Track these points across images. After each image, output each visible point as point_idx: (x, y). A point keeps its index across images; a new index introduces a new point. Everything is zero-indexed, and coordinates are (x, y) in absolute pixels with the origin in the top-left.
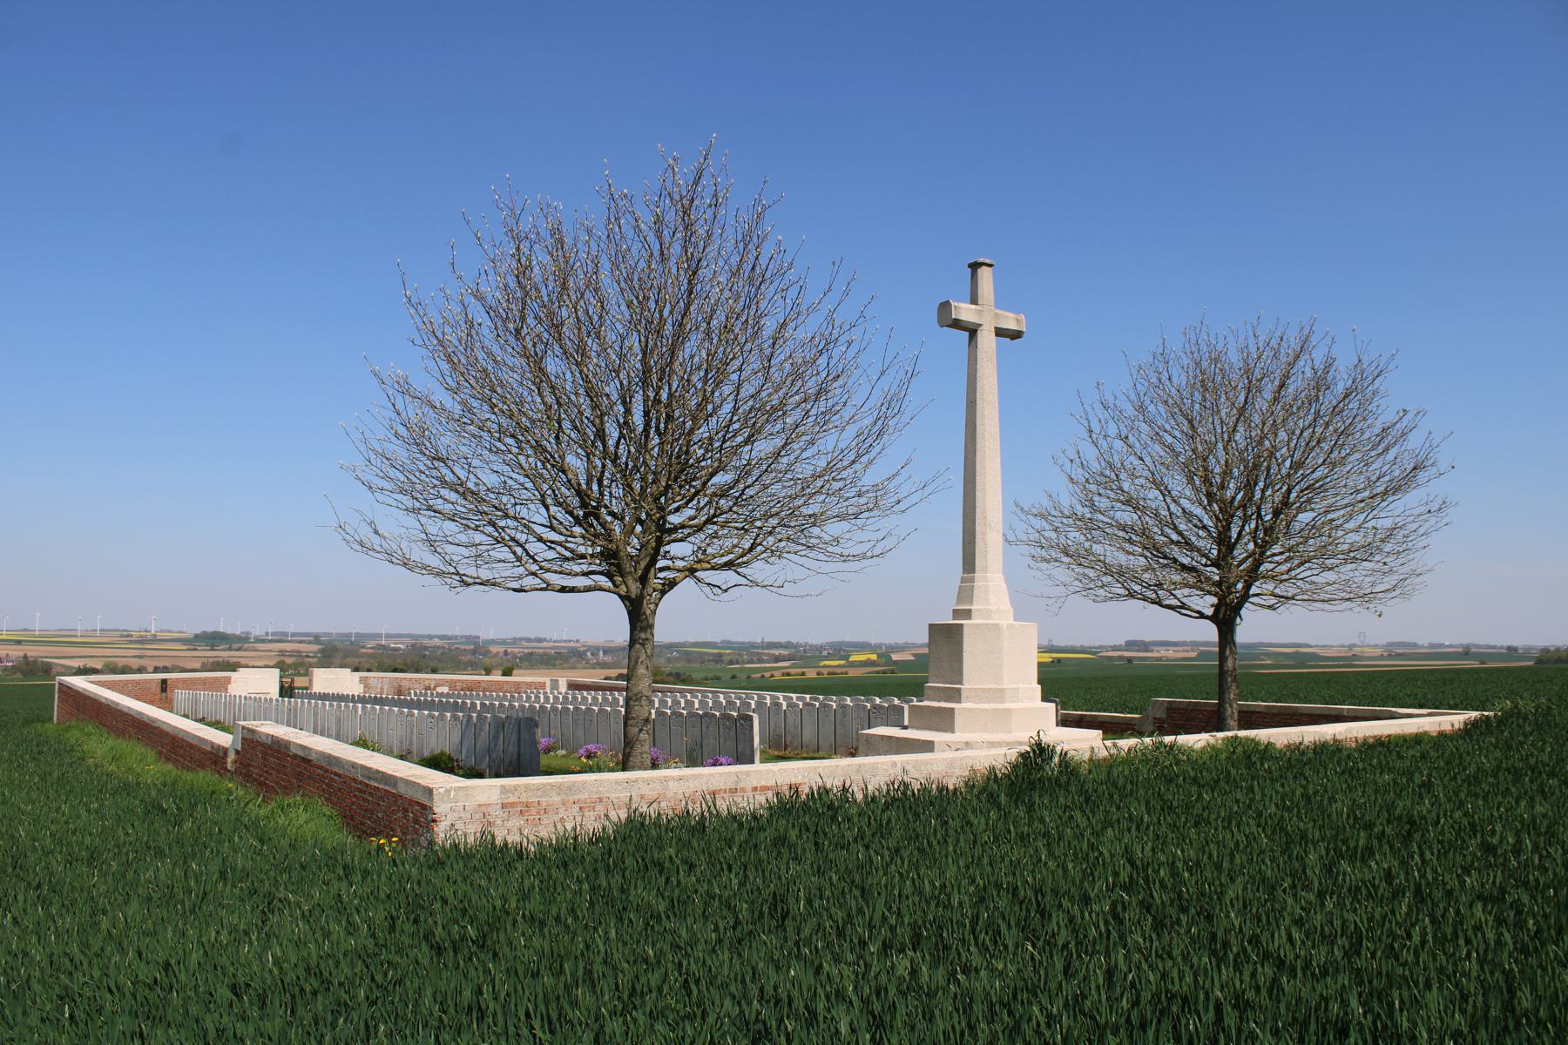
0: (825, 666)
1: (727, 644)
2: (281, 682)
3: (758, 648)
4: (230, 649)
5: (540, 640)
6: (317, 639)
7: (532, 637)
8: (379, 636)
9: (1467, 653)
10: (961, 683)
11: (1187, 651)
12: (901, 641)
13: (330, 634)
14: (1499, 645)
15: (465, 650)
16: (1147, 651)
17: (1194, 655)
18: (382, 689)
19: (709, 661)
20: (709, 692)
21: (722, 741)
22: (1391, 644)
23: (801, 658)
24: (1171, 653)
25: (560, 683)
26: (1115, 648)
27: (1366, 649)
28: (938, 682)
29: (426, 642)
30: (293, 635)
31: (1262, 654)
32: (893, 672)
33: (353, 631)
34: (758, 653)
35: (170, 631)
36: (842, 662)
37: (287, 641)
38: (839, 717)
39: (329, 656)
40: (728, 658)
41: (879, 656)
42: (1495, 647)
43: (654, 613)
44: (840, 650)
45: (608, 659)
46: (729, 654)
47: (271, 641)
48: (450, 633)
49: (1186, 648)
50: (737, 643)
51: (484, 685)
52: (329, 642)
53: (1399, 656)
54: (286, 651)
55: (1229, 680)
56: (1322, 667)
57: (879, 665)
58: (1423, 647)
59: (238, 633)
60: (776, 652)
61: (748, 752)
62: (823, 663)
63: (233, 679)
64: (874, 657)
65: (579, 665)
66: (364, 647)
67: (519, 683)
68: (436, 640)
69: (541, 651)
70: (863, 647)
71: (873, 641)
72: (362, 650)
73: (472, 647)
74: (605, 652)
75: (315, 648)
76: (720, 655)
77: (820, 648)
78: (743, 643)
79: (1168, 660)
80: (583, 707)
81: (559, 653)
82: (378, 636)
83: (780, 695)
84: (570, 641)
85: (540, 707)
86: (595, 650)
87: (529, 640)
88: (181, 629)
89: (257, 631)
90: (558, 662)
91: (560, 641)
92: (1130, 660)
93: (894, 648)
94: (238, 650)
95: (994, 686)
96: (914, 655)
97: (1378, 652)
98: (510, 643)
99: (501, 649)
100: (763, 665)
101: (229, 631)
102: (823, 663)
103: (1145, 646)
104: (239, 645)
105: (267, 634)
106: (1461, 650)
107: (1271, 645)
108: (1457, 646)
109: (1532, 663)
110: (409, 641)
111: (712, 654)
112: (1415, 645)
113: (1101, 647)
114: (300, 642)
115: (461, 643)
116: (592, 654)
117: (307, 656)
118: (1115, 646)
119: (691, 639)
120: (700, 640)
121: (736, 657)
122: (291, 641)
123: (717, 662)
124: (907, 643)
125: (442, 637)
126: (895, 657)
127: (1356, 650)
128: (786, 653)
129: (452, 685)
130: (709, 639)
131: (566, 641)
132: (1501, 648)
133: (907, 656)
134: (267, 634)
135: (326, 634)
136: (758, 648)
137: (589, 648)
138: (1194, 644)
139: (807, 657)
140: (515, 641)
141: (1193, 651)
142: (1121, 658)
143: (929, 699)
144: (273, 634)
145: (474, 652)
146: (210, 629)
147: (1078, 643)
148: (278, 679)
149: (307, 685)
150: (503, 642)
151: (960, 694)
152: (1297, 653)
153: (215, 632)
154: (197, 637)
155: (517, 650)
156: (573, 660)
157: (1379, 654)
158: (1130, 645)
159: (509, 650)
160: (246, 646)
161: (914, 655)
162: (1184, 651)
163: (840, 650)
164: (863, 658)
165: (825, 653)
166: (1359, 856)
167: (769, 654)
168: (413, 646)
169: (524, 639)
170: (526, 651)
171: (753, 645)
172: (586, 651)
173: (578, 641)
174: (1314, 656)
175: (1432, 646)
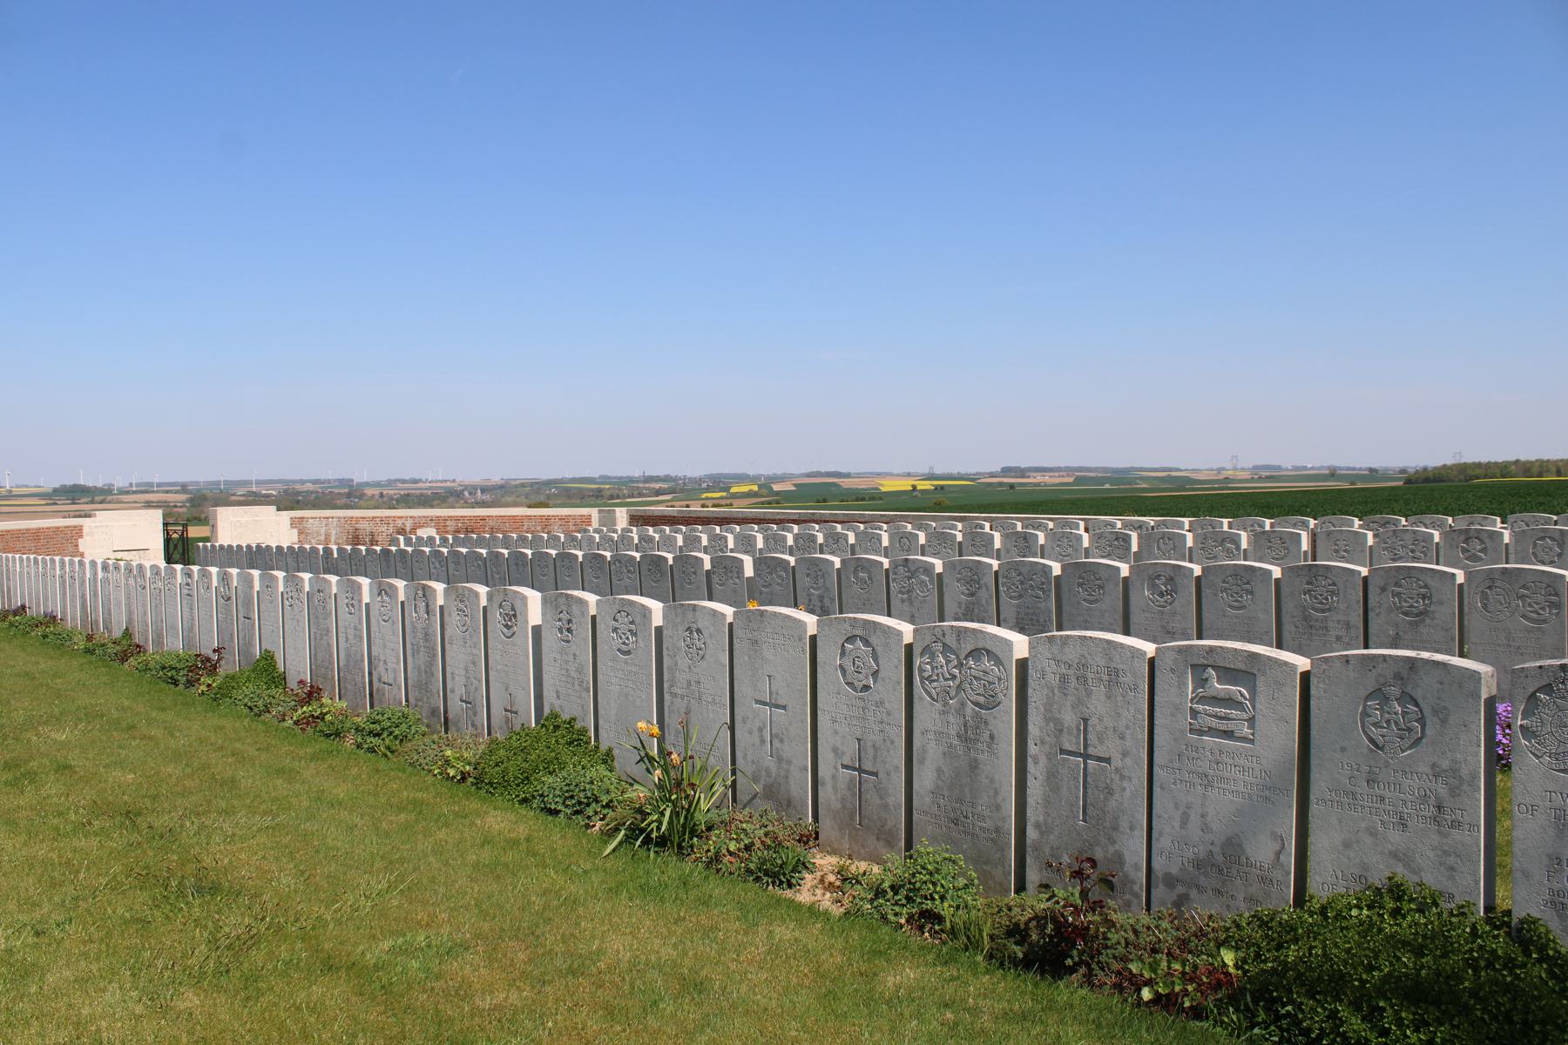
0: (707, 498)
1: (605, 479)
2: (166, 532)
3: (637, 482)
4: (92, 502)
5: (415, 481)
6: (184, 488)
7: (407, 478)
8: (249, 483)
9: (1333, 474)
11: (1063, 476)
12: (779, 472)
13: (197, 483)
14: (1358, 466)
15: (339, 493)
16: (1023, 477)
17: (1071, 480)
18: (327, 537)
19: (589, 496)
20: (1017, 519)
22: (1257, 468)
23: (682, 491)
25: (618, 514)
26: (992, 475)
29: (298, 487)
30: (159, 485)
31: (1137, 478)
33: (222, 479)
34: (638, 487)
35: (27, 486)
36: (724, 494)
37: (153, 492)
39: (199, 505)
40: (608, 493)
41: (760, 486)
42: (1354, 469)
44: (719, 482)
45: (487, 497)
46: (608, 489)
47: (134, 492)
48: (322, 477)
49: (1061, 474)
50: (615, 478)
51: (491, 523)
52: (198, 490)
54: (153, 502)
56: (1215, 489)
57: (762, 496)
58: (1287, 470)
59: (100, 485)
60: (657, 486)
62: (704, 495)
63: (85, 530)
64: (755, 488)
65: (457, 505)
66: (233, 495)
67: (548, 518)
68: (310, 485)
69: (418, 492)
70: (742, 478)
71: (751, 473)
72: (233, 498)
73: (347, 490)
74: (483, 491)
75: (183, 497)
76: (600, 490)
77: (700, 481)
78: (621, 478)
79: (1046, 485)
80: (553, 552)
81: (436, 493)
82: (248, 483)
84: (446, 481)
85: (367, 550)
86: (472, 489)
87: (404, 481)
88: (38, 484)
89: (120, 482)
90: (435, 503)
91: (436, 482)
92: (1012, 486)
93: (775, 478)
94: (101, 503)
98: (383, 486)
99: (376, 491)
100: (645, 499)
101: (90, 484)
102: (704, 495)
103: (1021, 472)
104: (102, 498)
105: (131, 485)
106: (1327, 472)
109: (1401, 483)
110: (281, 486)
111: (592, 490)
112: (1279, 468)
113: (978, 474)
114: (167, 492)
115: (336, 487)
116: (470, 494)
117: (175, 506)
118: (992, 473)
119: (568, 475)
120: (578, 476)
121: (617, 491)
122: (157, 492)
123: (597, 497)
124: (785, 474)
125: (315, 482)
126: (776, 488)
127: (1230, 473)
128: (666, 486)
129: (440, 524)
130: (586, 474)
131: (442, 481)
132: (1360, 469)
133: (788, 487)
134: (131, 485)
135: (192, 483)
136: (637, 482)
137: (466, 487)
139: (688, 490)
140: (391, 483)
141: (1068, 476)
142: (1001, 484)
144: (137, 485)
145: (349, 495)
146: (69, 482)
147: (955, 471)
148: (161, 526)
149: (208, 534)
150: (378, 484)
152: (1169, 476)
153: (74, 485)
154: (55, 490)
155: (392, 492)
156: (450, 500)
157: (1250, 477)
158: (1006, 471)
159: (385, 492)
160: (109, 498)
162: (1059, 476)
163: (719, 482)
164: (745, 489)
165: (704, 485)
166: (18, 561)
167: (649, 489)
168: (285, 491)
169: (399, 480)
170: (402, 493)
171: (632, 480)
172: (463, 490)
173: (454, 481)
175: (1296, 468)
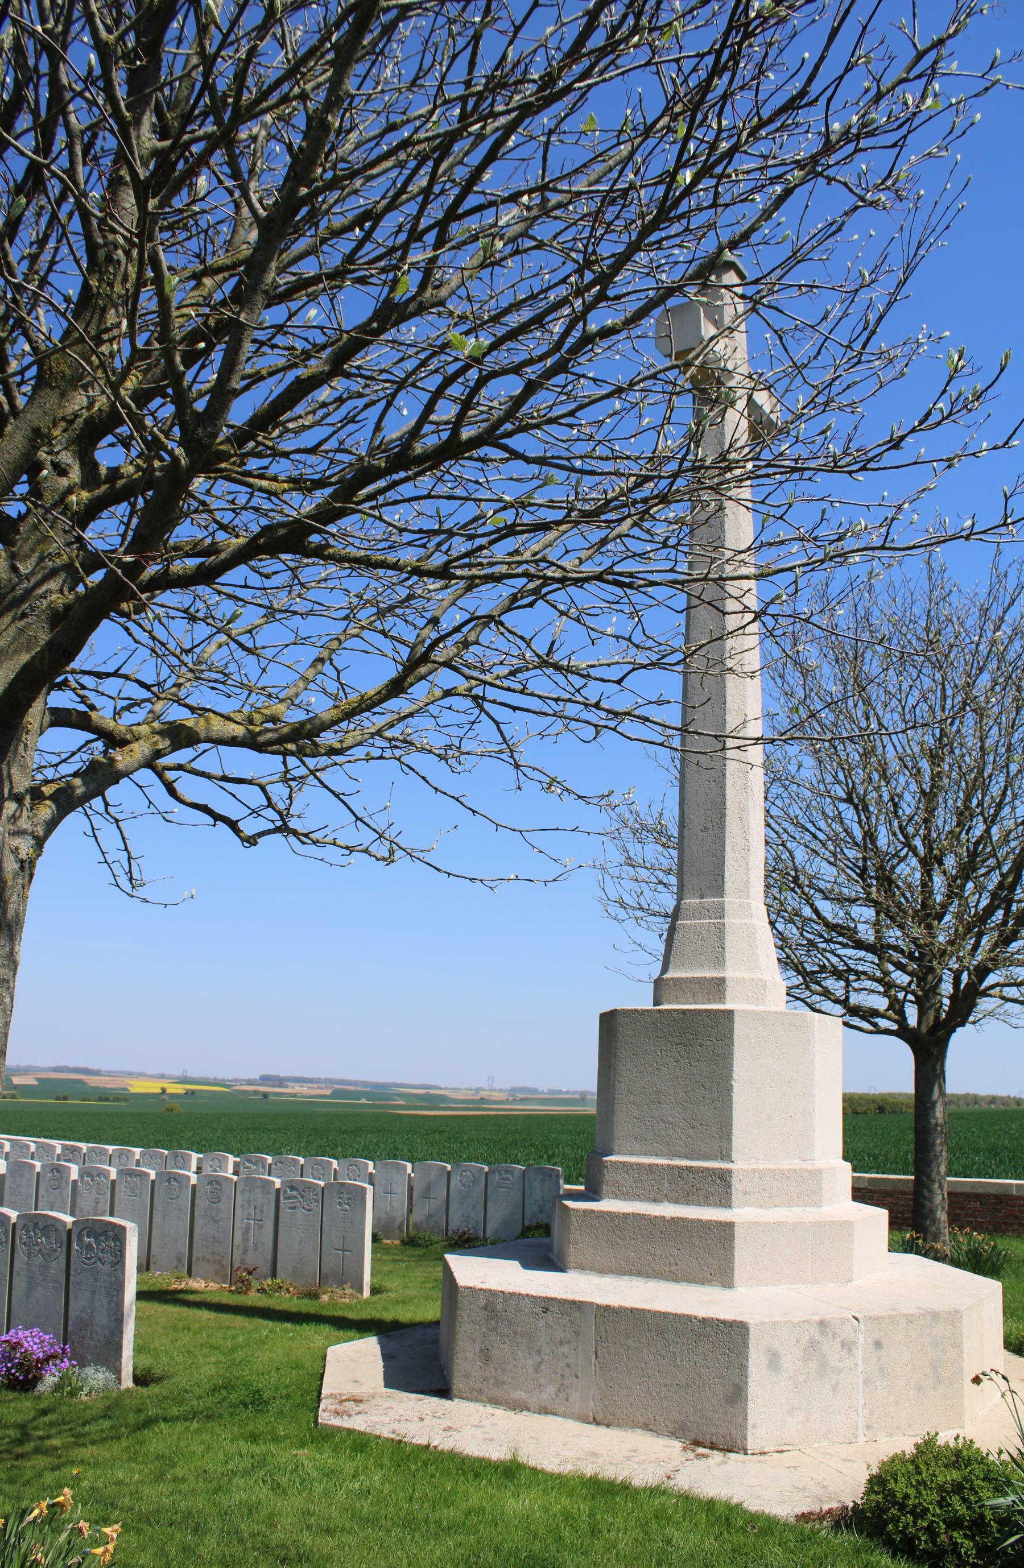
10: (726, 1155)
17: (329, 1092)
21: (20, 1284)
22: (514, 1090)
24: (305, 1089)
26: (249, 1082)
27: (493, 1094)
28: (646, 1154)
32: (14, 1097)
38: (202, 1202)
43: (27, 867)
53: (524, 1100)
55: (938, 1141)
61: (102, 1319)
83: (31, 1143)
92: (265, 1095)
95: (797, 1164)
96: (37, 1079)
97: (503, 1096)
103: (280, 1081)
107: (402, 1086)
108: (573, 1093)
126: (17, 1080)
133: (30, 1081)
138: (328, 1081)
142: (256, 1093)
143: (619, 1195)
147: (211, 1075)
151: (729, 1186)
152: (428, 1094)
158: (265, 1079)
161: (37, 1079)
174: (443, 1098)
175: (551, 1092)
